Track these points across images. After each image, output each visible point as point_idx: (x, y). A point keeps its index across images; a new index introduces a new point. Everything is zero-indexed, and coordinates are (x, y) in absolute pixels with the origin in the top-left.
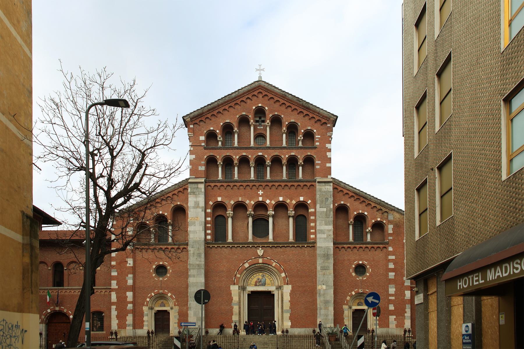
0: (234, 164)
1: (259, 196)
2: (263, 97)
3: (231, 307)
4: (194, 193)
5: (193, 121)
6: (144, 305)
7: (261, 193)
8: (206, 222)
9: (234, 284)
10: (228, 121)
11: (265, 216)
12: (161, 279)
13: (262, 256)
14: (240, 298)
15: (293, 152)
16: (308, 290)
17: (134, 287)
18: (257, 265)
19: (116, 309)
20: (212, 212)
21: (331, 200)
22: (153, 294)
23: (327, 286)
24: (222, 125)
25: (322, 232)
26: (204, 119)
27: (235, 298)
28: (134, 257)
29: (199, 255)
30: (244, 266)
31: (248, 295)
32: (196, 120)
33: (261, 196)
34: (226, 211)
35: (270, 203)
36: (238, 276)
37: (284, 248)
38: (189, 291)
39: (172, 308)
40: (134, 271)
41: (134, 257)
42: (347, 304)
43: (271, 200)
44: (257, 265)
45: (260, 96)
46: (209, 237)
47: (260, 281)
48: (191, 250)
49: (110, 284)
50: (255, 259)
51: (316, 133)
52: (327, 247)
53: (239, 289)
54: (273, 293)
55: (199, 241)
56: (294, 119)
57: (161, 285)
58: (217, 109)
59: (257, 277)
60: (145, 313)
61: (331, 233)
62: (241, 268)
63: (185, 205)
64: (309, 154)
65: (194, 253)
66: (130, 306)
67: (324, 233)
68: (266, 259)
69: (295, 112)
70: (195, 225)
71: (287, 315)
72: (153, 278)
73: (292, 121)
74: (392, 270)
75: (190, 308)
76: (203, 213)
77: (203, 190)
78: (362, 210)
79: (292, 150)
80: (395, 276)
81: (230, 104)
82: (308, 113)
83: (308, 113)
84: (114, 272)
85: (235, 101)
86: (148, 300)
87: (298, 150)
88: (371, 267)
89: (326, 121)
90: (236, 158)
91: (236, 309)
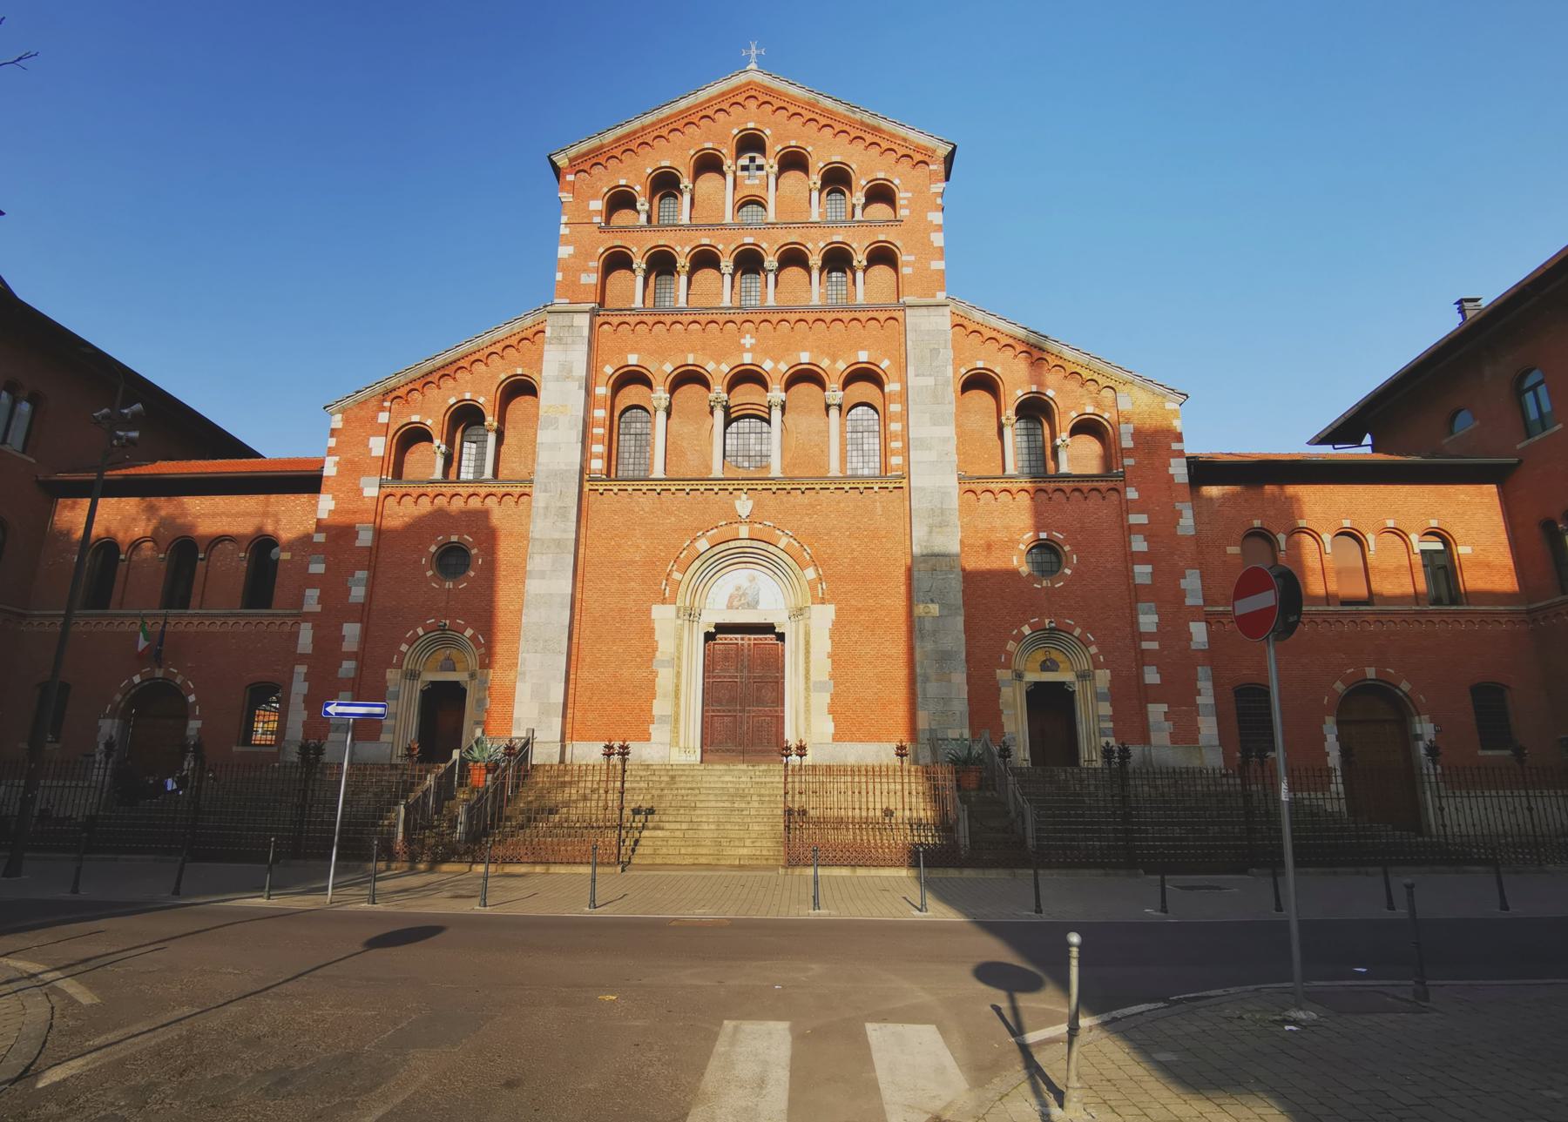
1: (743, 349)
4: (560, 340)
6: (390, 665)
7: (748, 341)
9: (664, 601)
12: (449, 585)
23: (942, 606)
27: (665, 646)
30: (695, 548)
33: (748, 351)
35: (775, 369)
36: (677, 576)
42: (1007, 666)
43: (776, 361)
45: (752, 104)
47: (744, 594)
48: (540, 498)
53: (678, 617)
55: (566, 471)
61: (952, 447)
62: (685, 552)
65: (547, 508)
68: (761, 526)
71: (822, 699)
74: (1143, 558)
75: (524, 673)
86: (404, 648)
91: (664, 678)
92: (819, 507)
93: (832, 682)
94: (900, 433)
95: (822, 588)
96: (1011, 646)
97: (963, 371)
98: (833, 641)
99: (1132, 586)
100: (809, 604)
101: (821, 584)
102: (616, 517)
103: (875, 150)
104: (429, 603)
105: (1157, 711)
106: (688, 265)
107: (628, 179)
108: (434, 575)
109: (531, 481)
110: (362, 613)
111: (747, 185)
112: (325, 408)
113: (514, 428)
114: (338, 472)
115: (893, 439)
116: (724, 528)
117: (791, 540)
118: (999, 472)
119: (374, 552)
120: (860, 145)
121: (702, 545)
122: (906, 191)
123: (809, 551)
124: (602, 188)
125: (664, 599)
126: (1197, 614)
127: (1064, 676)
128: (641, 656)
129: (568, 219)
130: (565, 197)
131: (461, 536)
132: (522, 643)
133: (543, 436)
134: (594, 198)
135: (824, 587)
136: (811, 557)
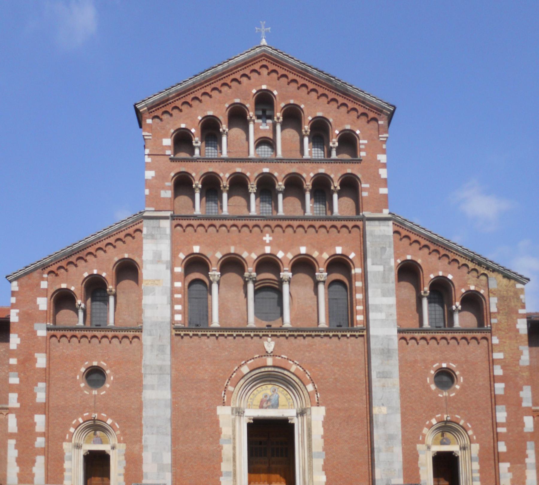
0: (220, 187)
1: (264, 244)
2: (269, 74)
3: (219, 446)
4: (152, 237)
5: (151, 112)
6: (64, 440)
7: (267, 238)
8: (173, 291)
9: (224, 404)
10: (210, 113)
11: (271, 281)
12: (95, 392)
13: (272, 352)
14: (234, 431)
15: (322, 168)
16: (355, 416)
17: (47, 407)
18: (263, 370)
19: (17, 447)
20: (183, 272)
21: (390, 251)
22: (81, 421)
23: (389, 408)
24: (201, 121)
25: (378, 309)
26: (169, 110)
27: (226, 431)
28: (48, 351)
29: (161, 349)
30: (241, 372)
31: (249, 425)
32: (156, 110)
33: (268, 245)
34: (208, 270)
35: (285, 257)
36: (230, 388)
37: (310, 338)
38: (144, 414)
39: (113, 448)
40: (47, 375)
41: (48, 351)
42: (423, 442)
43: (286, 252)
44: (263, 370)
45: (264, 72)
46: (178, 317)
47: (269, 400)
48: (146, 339)
49: (6, 401)
50: (261, 358)
51: (360, 136)
52: (387, 335)
53: (232, 414)
54: (292, 422)
55: (162, 322)
56: (322, 111)
57: (95, 403)
58: (191, 93)
59: (264, 392)
60: (67, 454)
61: (394, 311)
62: (235, 374)
63: (137, 259)
64: (349, 171)
65: (152, 346)
66: (40, 442)
67: (381, 311)
68: (280, 358)
69: (324, 100)
70: (154, 294)
71: (319, 463)
72: (81, 390)
73: (320, 114)
74: (501, 379)
75: (147, 446)
76: (169, 272)
77: (168, 231)
78: (443, 271)
79: (320, 165)
80: (505, 389)
81: (215, 84)
82: (345, 101)
83: (345, 101)
84: (14, 377)
85: (222, 79)
86: (72, 430)
87: (330, 164)
88: (463, 373)
89: (376, 116)
90: (225, 177)
91: (227, 450)
92: (314, 347)
93: (324, 453)
94: (362, 300)
95: (317, 397)
96: (425, 430)
97: (399, 261)
98: (324, 429)
99: (493, 396)
100: (310, 406)
101: (317, 394)
102: (192, 351)
103: (343, 109)
104: (84, 403)
105: (504, 467)
106: (228, 186)
107: (186, 123)
108: (85, 386)
109: (140, 330)
110: (44, 409)
111: (261, 129)
112: (6, 277)
113: (123, 292)
114: (20, 319)
115: (358, 304)
116: (258, 359)
117: (298, 367)
118: (417, 327)
119: (47, 371)
120: (334, 105)
121: (245, 369)
122: (364, 139)
123: (309, 374)
124: (170, 129)
125: (224, 403)
126: (529, 412)
127: (453, 448)
128: (212, 437)
129: (150, 151)
130: (147, 136)
131: (99, 362)
132: (144, 428)
133: (147, 300)
134: (166, 137)
135: (319, 396)
136: (310, 378)
